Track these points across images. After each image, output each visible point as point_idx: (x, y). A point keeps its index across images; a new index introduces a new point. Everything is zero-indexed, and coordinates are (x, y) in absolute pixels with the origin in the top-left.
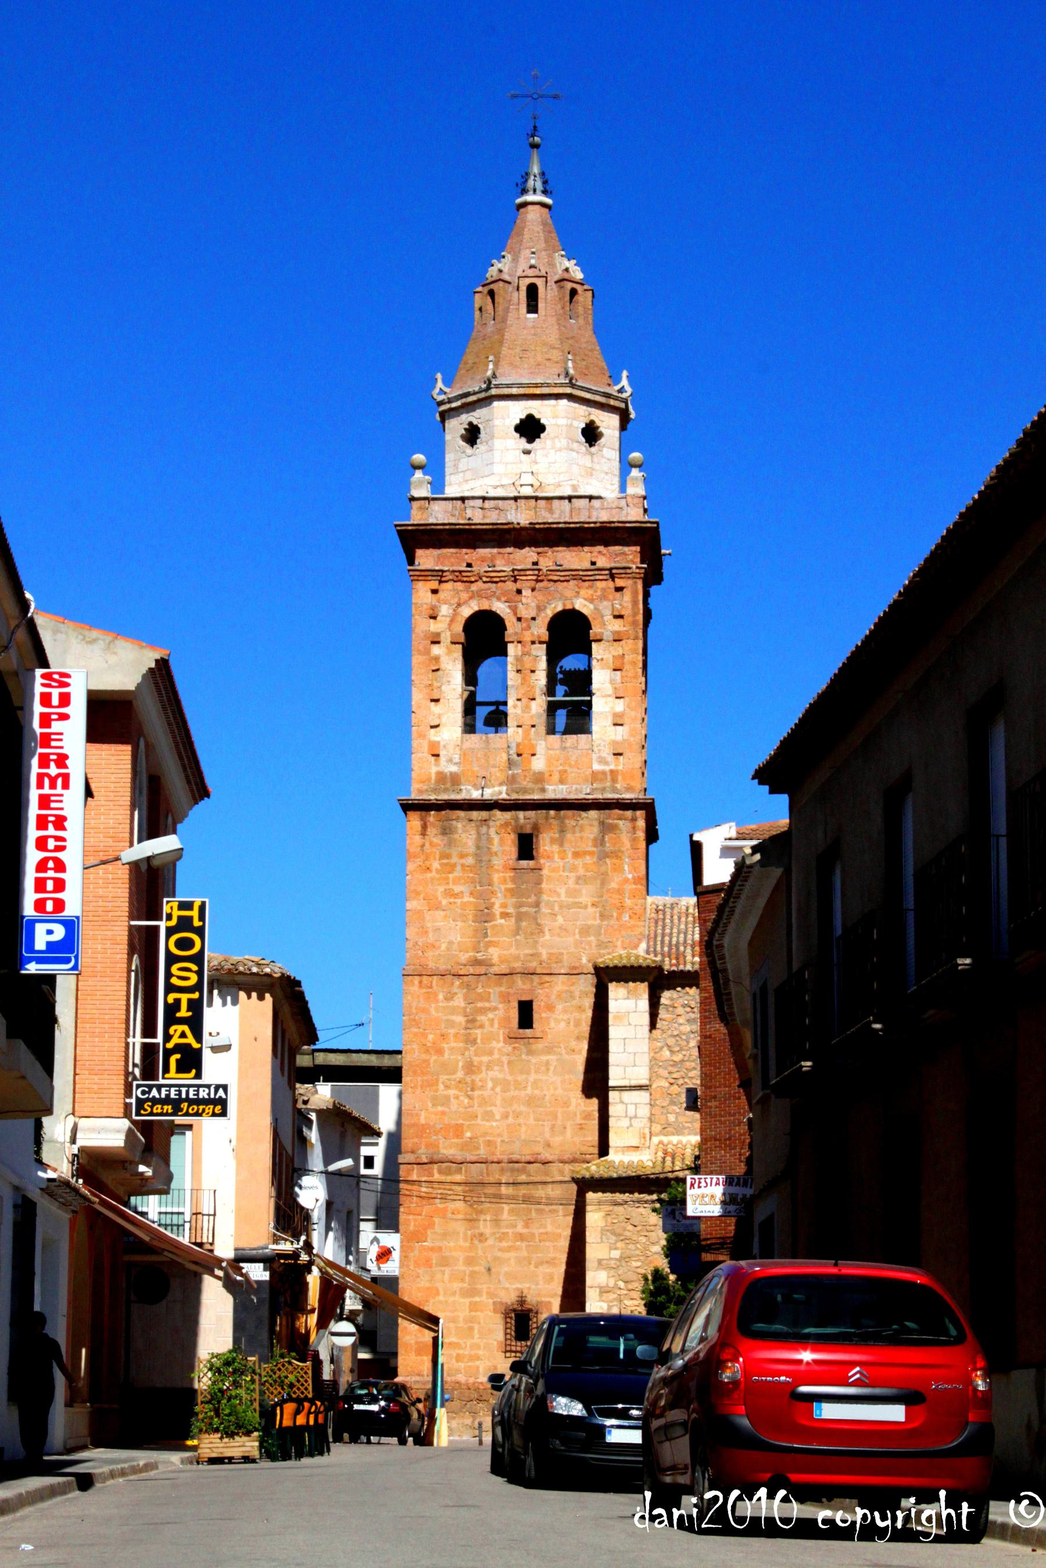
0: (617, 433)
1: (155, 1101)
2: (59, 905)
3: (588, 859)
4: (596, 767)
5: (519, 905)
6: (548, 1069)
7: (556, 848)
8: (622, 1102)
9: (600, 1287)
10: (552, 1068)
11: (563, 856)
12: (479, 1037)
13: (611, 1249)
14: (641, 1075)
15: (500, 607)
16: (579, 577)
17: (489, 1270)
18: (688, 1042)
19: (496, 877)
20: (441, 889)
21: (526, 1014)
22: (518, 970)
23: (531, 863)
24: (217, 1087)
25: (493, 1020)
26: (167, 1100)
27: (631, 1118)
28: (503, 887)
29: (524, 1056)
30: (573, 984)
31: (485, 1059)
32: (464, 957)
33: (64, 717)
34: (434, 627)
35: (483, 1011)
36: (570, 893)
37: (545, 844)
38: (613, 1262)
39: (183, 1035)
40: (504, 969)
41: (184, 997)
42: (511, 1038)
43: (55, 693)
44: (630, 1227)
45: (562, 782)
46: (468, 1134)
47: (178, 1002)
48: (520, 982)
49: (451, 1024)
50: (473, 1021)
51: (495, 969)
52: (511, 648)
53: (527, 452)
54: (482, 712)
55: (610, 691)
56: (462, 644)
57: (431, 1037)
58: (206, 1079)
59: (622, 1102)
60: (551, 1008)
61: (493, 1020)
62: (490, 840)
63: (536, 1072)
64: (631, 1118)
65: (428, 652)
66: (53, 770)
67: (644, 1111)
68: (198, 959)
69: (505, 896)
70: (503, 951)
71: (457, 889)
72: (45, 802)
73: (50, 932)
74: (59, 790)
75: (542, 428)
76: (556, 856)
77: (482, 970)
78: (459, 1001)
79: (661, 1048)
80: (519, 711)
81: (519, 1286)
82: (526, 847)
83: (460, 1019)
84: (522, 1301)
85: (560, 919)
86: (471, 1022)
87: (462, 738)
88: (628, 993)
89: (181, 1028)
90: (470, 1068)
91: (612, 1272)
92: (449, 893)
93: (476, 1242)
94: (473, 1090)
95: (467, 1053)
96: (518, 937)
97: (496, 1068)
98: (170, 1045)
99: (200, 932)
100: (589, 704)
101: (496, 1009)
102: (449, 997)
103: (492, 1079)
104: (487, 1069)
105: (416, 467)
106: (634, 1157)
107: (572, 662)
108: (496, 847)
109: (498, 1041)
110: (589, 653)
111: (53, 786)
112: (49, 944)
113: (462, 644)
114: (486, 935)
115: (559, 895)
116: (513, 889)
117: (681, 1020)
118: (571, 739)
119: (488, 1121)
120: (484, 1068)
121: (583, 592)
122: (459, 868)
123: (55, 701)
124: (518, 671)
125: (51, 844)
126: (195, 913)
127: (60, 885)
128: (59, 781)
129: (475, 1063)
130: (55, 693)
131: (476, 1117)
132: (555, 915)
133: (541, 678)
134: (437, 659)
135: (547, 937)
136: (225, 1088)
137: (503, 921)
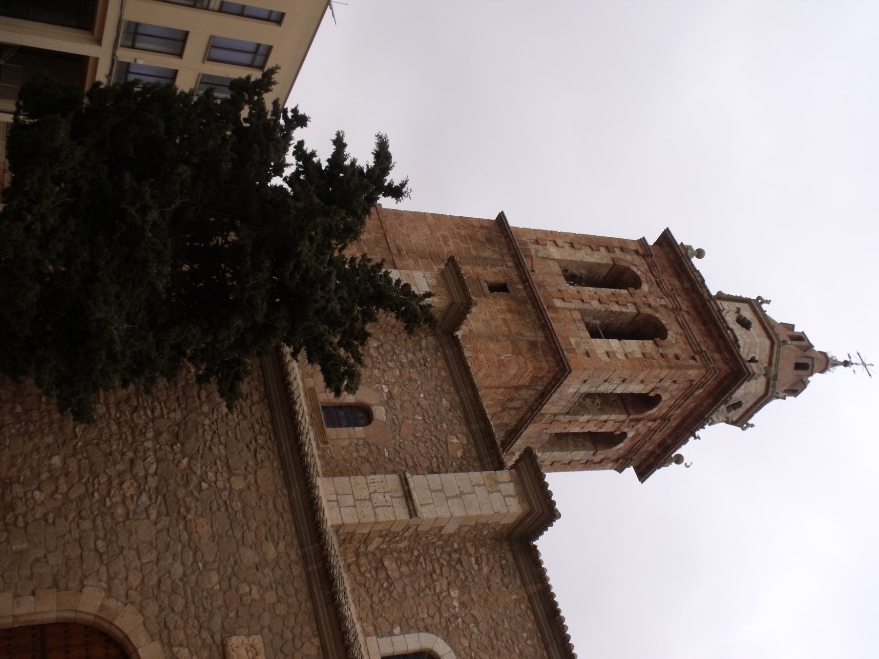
18: (391, 361)
27: (370, 499)
62: (493, 266)
114: (422, 258)
117: (410, 355)
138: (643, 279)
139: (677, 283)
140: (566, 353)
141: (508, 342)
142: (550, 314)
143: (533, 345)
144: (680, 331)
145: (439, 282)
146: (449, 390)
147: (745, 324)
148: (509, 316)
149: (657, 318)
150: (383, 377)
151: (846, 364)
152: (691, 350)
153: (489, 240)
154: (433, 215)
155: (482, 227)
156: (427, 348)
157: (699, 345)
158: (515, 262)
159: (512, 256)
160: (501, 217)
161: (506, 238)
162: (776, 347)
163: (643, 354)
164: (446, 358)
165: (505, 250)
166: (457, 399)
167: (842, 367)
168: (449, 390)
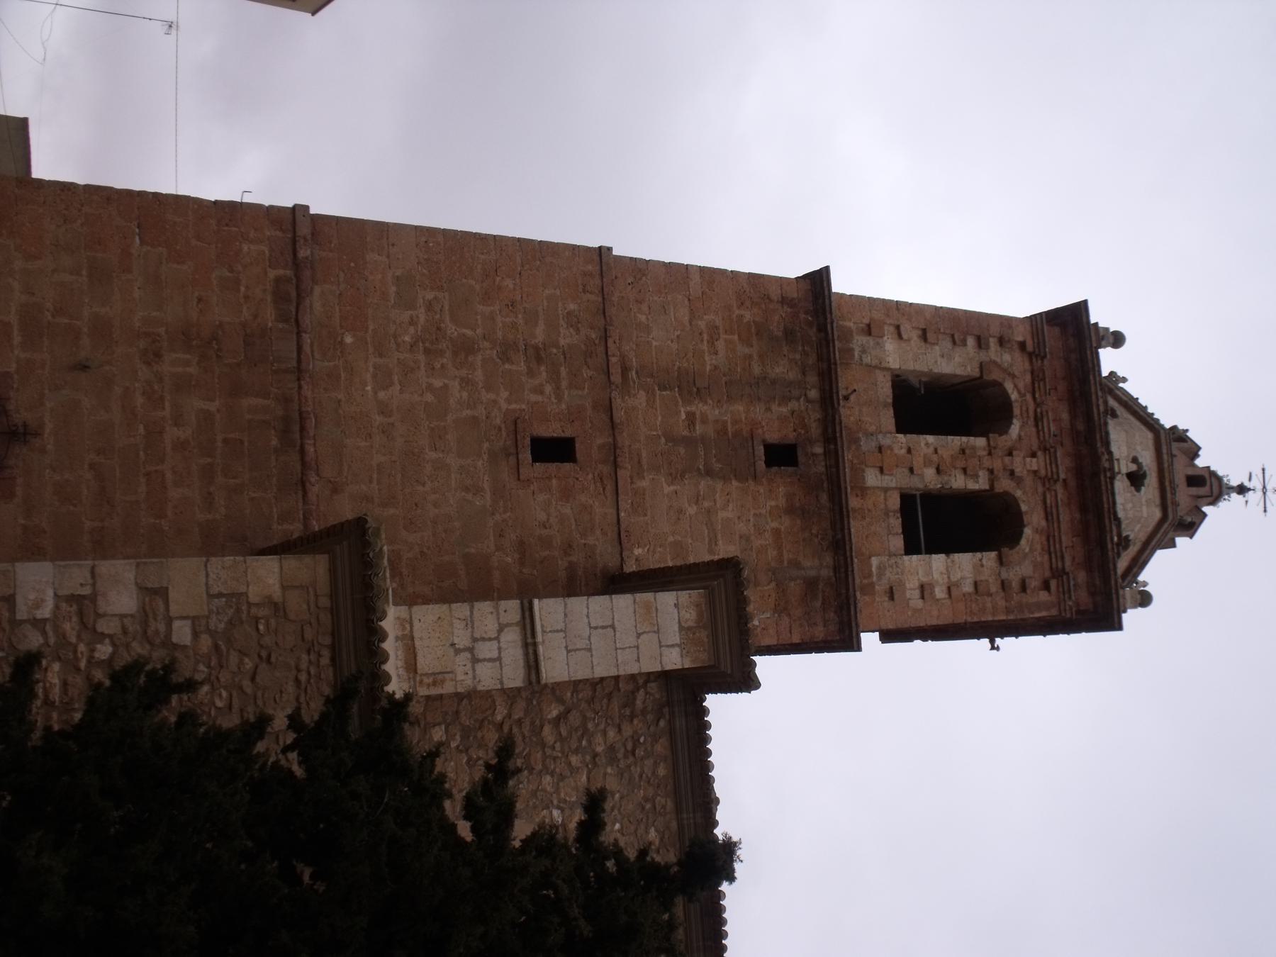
3: (772, 553)
4: (875, 561)
6: (467, 489)
7: (782, 502)
8: (501, 630)
9: (93, 598)
10: (469, 497)
12: (514, 367)
13: (194, 619)
16: (1050, 537)
17: (84, 367)
18: (576, 751)
19: (739, 408)
20: (718, 322)
21: (554, 450)
22: (619, 438)
23: (761, 464)
25: (542, 393)
27: (471, 650)
28: (727, 418)
29: (486, 445)
30: (604, 534)
31: (479, 375)
35: (555, 377)
38: (162, 628)
40: (619, 415)
42: (515, 424)
44: (249, 664)
46: (349, 339)
48: (599, 441)
50: (539, 360)
51: (617, 402)
55: (954, 579)
56: (981, 377)
57: (509, 283)
59: (501, 630)
60: (566, 494)
61: (542, 393)
62: (785, 400)
63: (462, 467)
64: (471, 650)
67: (487, 677)
69: (716, 421)
71: (720, 345)
76: (773, 503)
77: (616, 378)
78: (567, 338)
79: (561, 701)
80: (925, 450)
81: (49, 427)
83: (540, 334)
85: (692, 510)
86: (538, 355)
87: (889, 369)
88: (689, 629)
90: (464, 349)
91: (133, 627)
93: (142, 344)
94: (427, 352)
95: (487, 344)
96: (663, 440)
97: (465, 394)
100: (919, 552)
101: (559, 398)
102: (573, 321)
103: (446, 386)
104: (462, 379)
109: (508, 401)
113: (981, 377)
114: (663, 387)
115: (724, 508)
116: (726, 433)
117: (612, 733)
119: (374, 376)
120: (464, 372)
121: (1037, 537)
122: (747, 351)
124: (963, 451)
129: (470, 359)
131: (381, 356)
132: (697, 503)
134: (964, 343)
135: (668, 489)
137: (683, 416)
138: (1016, 411)
139: (1065, 416)
140: (858, 594)
141: (773, 585)
142: (854, 502)
143: (811, 585)
144: (1044, 523)
145: (700, 615)
146: (664, 807)
147: (1136, 479)
148: (786, 522)
149: (1015, 500)
150: (557, 791)
151: (1242, 490)
152: (1047, 566)
153: (789, 335)
154: (702, 270)
155: (784, 301)
156: (644, 712)
157: (1063, 558)
158: (822, 390)
159: (821, 375)
160: (819, 279)
161: (819, 330)
162: (1166, 525)
163: (976, 584)
164: (672, 732)
165: (812, 360)
166: (674, 825)
167: (1234, 495)
168: (664, 807)
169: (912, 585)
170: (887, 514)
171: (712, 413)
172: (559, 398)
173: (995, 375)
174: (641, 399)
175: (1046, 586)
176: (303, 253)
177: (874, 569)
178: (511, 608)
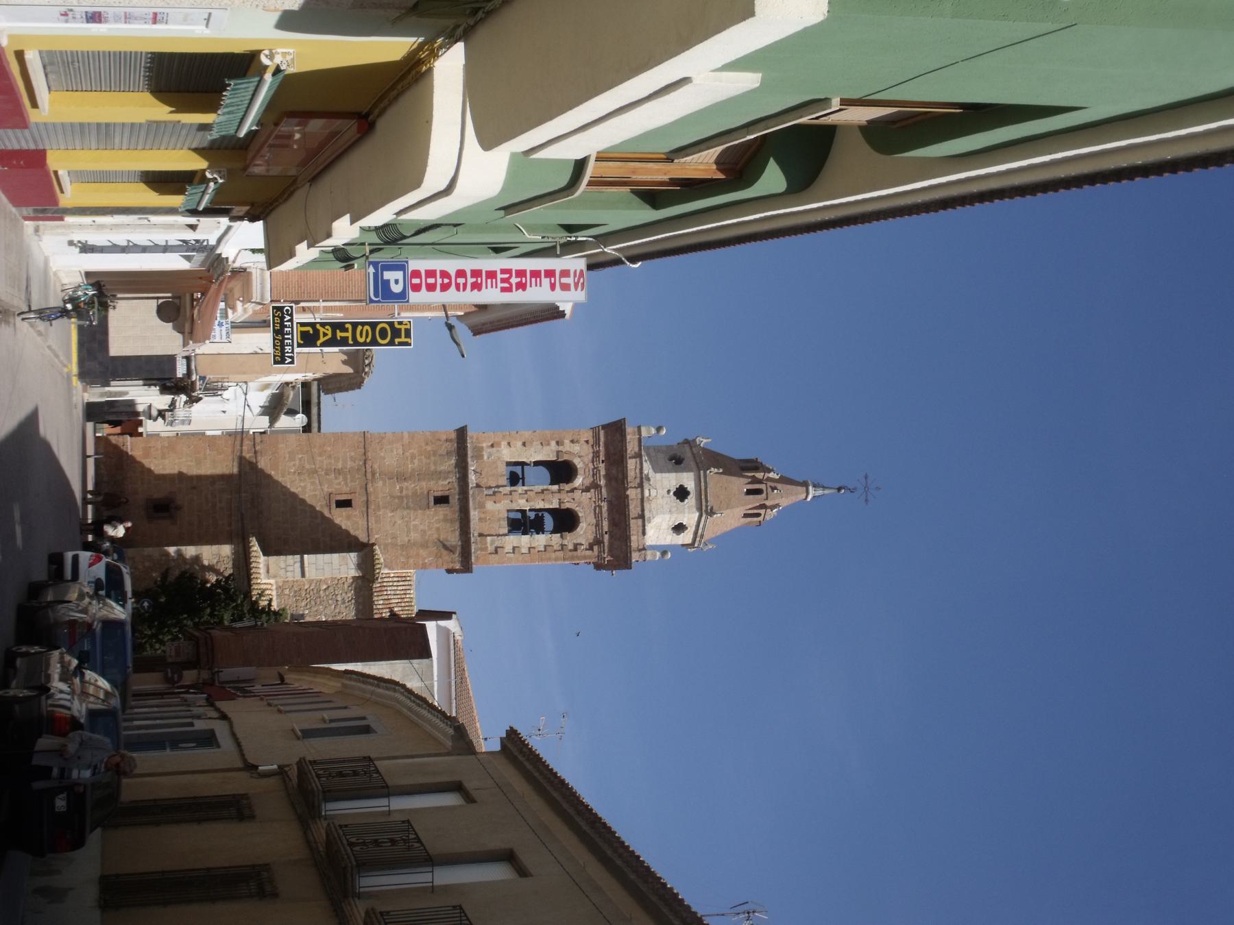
0: (680, 543)
1: (282, 318)
2: (417, 288)
5: (407, 496)
7: (441, 517)
11: (438, 521)
14: (311, 573)
15: (578, 481)
19: (424, 484)
24: (292, 358)
26: (283, 326)
32: (376, 466)
33: (553, 287)
34: (567, 442)
35: (345, 479)
36: (415, 526)
37: (442, 510)
39: (325, 335)
40: (370, 489)
41: (349, 334)
43: (569, 281)
45: (480, 519)
47: (346, 330)
49: (337, 459)
51: (369, 485)
52: (555, 487)
53: (669, 492)
54: (518, 470)
58: (297, 350)
62: (445, 479)
65: (552, 439)
66: (514, 280)
68: (374, 342)
70: (381, 490)
71: (416, 461)
72: (491, 275)
73: (397, 282)
74: (500, 285)
75: (682, 500)
77: (369, 476)
78: (349, 464)
82: (442, 500)
83: (340, 466)
84: (178, 508)
85: (399, 522)
86: (338, 472)
89: (330, 333)
92: (413, 457)
98: (318, 326)
99: (391, 343)
101: (346, 484)
102: (353, 459)
105: (659, 429)
106: (262, 570)
107: (549, 522)
108: (441, 482)
110: (554, 532)
111: (503, 281)
112: (388, 281)
118: (505, 523)
123: (564, 280)
125: (461, 281)
126: (403, 339)
127: (431, 288)
128: (506, 285)
130: (569, 281)
133: (540, 505)
134: (549, 444)
136: (292, 362)
169: (509, 548)
170: (499, 520)
171: (410, 486)
172: (346, 484)
173: (566, 457)
174: (380, 483)
175: (591, 548)
176: (258, 448)
177: (190, 551)
178: (298, 557)
